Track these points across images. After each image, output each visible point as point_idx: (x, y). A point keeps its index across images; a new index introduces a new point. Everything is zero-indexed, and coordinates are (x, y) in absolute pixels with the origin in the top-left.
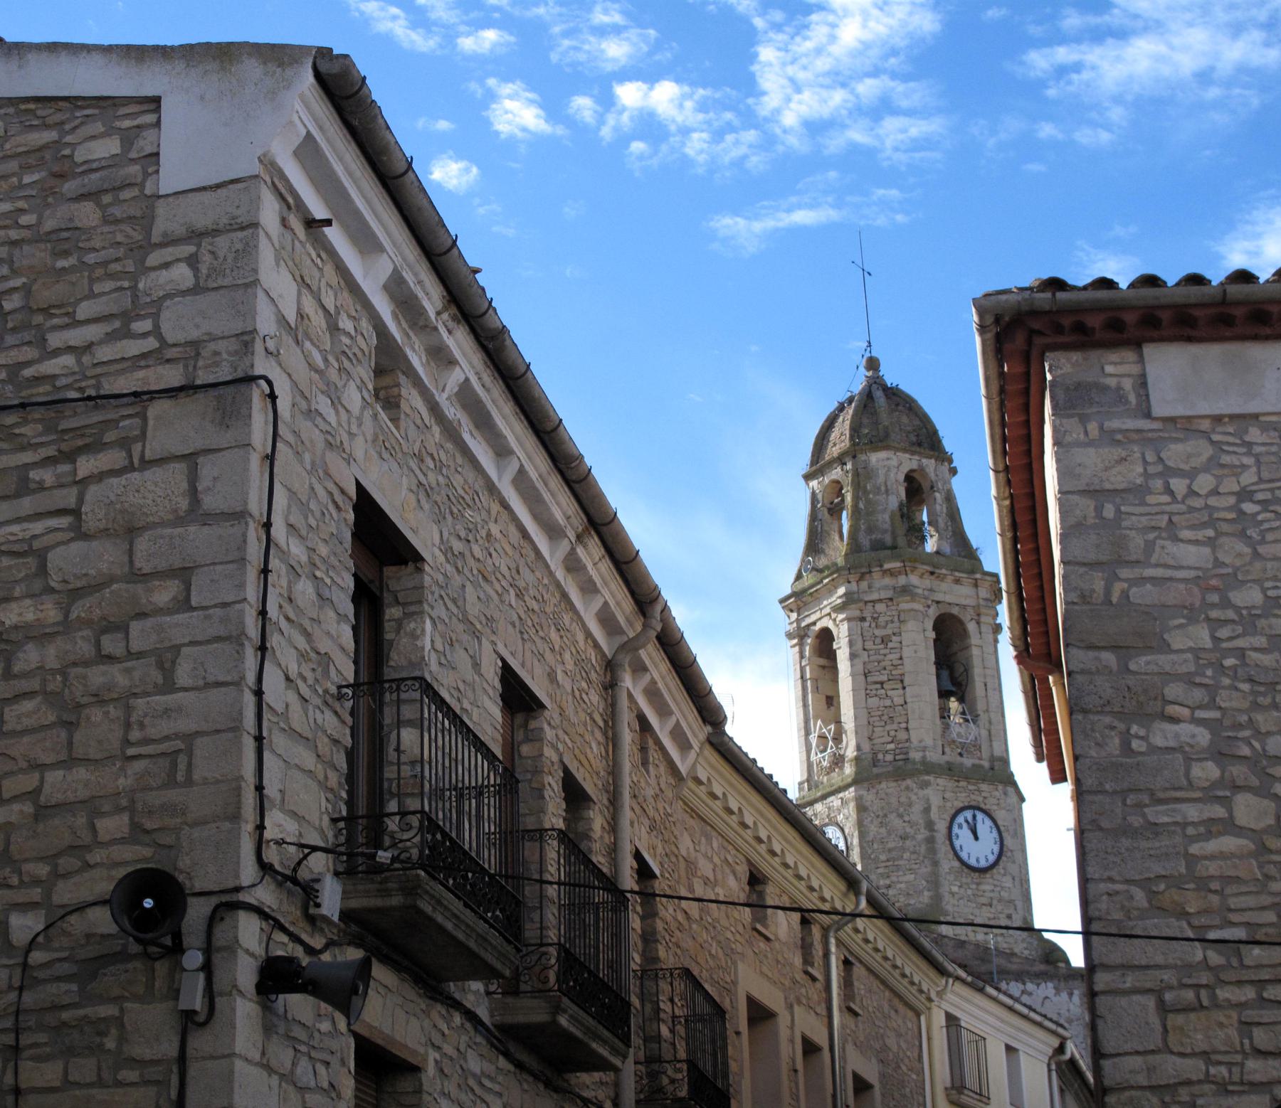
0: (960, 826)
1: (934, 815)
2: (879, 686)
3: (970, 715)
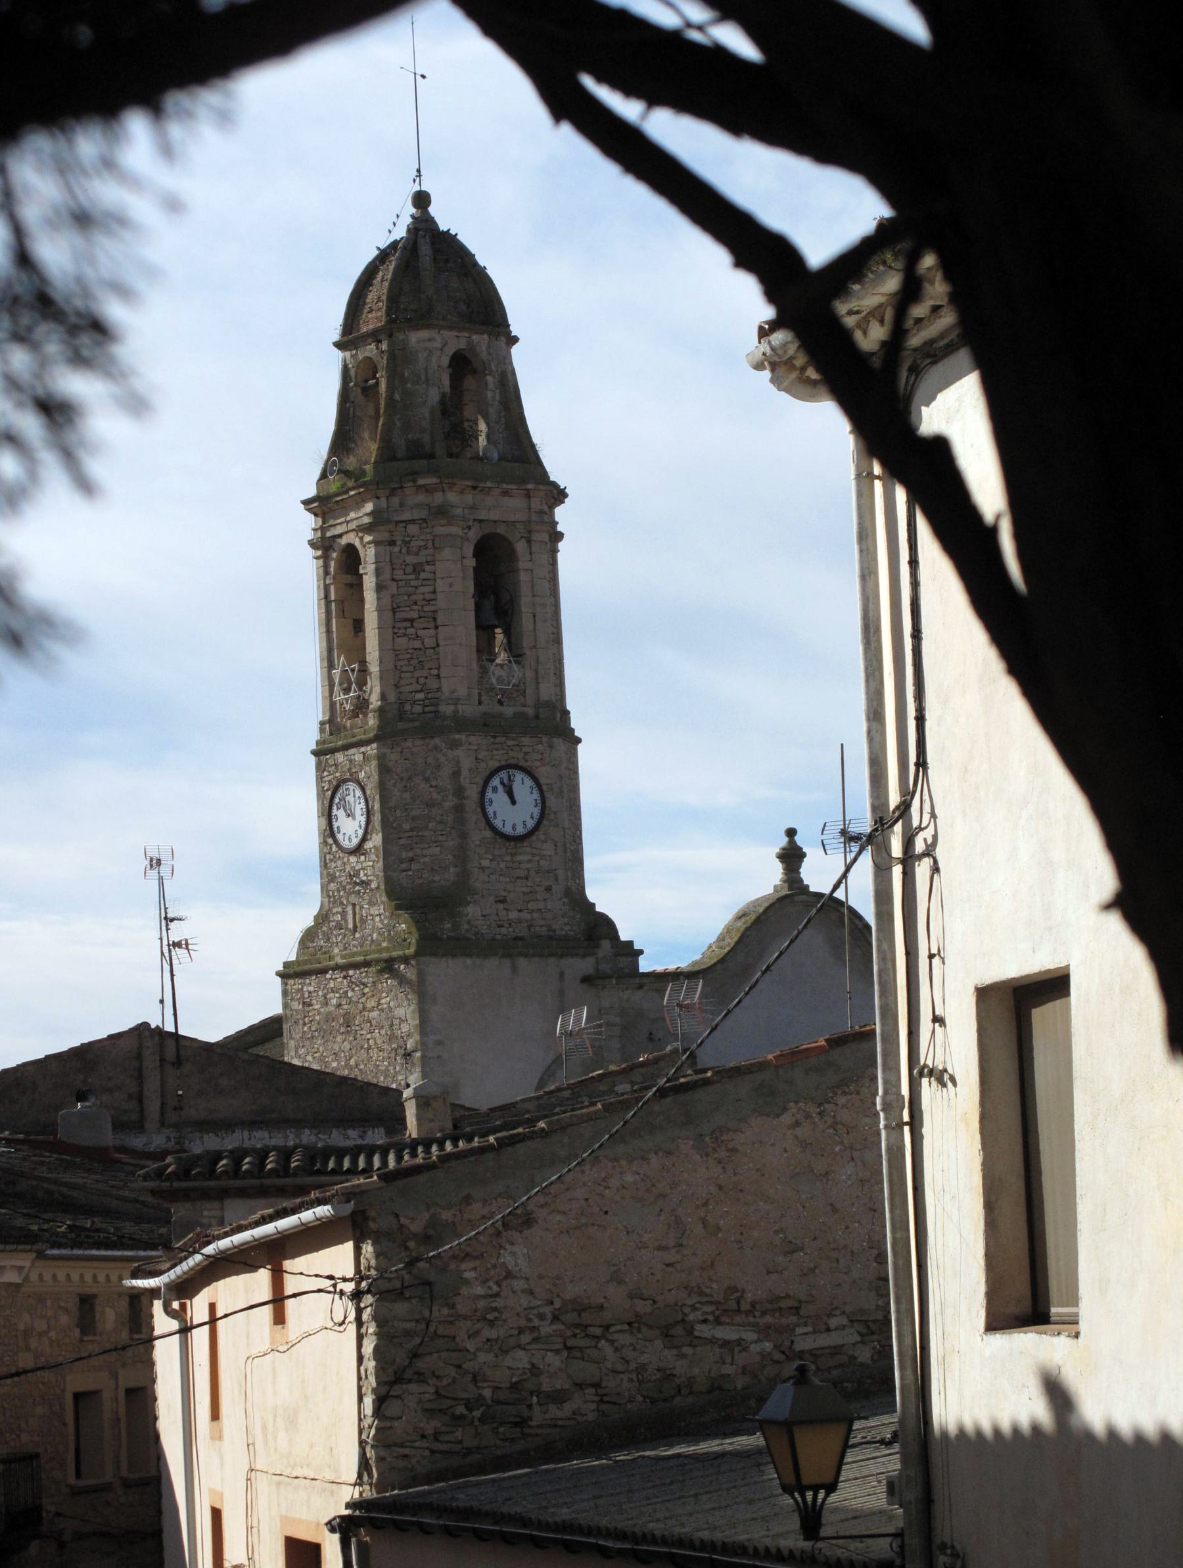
0: (495, 790)
2: (408, 624)
3: (516, 653)
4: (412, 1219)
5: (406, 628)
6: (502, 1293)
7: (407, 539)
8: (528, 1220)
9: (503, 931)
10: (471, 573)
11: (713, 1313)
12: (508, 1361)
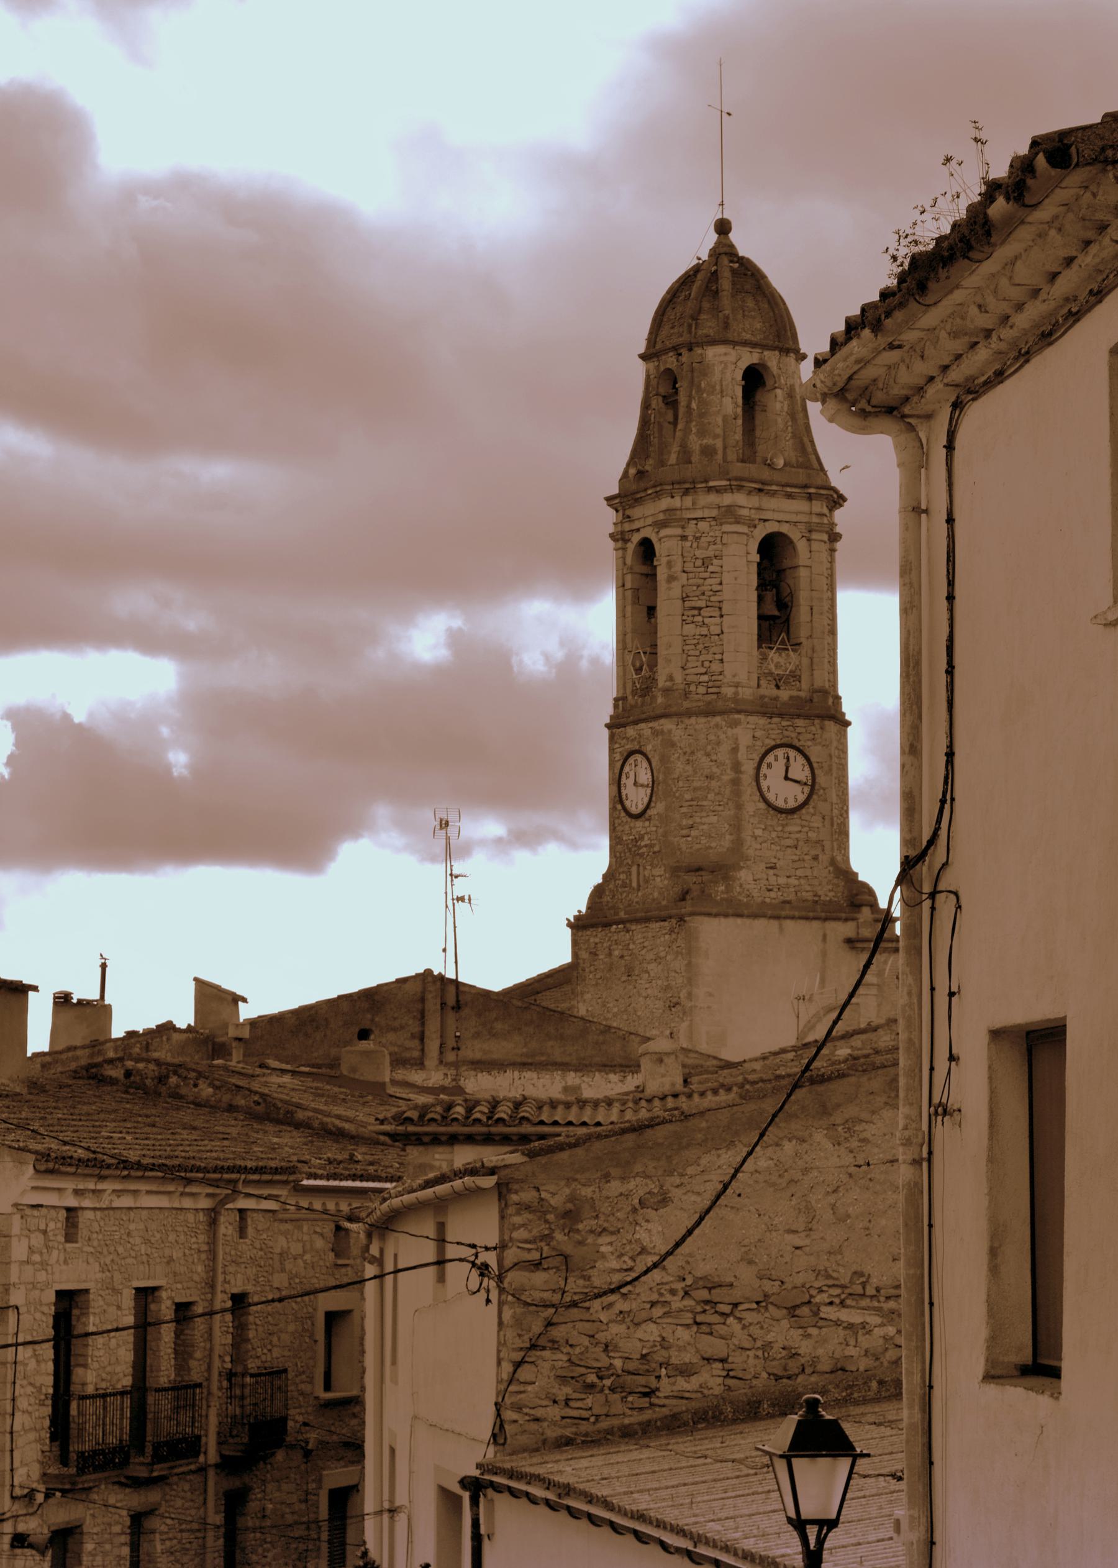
1: (742, 755)
2: (696, 612)
4: (553, 1194)
5: (693, 616)
6: (635, 1268)
7: (698, 535)
8: (664, 1199)
9: (773, 895)
10: (754, 568)
11: (838, 1296)
12: (639, 1334)
